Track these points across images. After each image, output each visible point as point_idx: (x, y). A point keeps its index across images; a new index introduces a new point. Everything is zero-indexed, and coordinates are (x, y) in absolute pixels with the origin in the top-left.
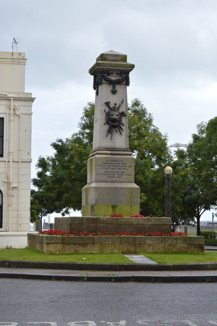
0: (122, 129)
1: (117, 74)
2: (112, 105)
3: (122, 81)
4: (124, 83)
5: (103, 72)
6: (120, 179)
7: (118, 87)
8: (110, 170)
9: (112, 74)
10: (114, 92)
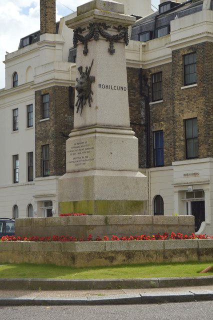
0: (91, 99)
1: (114, 28)
2: (84, 70)
3: (120, 39)
4: (122, 41)
5: (100, 24)
7: (117, 47)
8: (77, 156)
9: (109, 27)
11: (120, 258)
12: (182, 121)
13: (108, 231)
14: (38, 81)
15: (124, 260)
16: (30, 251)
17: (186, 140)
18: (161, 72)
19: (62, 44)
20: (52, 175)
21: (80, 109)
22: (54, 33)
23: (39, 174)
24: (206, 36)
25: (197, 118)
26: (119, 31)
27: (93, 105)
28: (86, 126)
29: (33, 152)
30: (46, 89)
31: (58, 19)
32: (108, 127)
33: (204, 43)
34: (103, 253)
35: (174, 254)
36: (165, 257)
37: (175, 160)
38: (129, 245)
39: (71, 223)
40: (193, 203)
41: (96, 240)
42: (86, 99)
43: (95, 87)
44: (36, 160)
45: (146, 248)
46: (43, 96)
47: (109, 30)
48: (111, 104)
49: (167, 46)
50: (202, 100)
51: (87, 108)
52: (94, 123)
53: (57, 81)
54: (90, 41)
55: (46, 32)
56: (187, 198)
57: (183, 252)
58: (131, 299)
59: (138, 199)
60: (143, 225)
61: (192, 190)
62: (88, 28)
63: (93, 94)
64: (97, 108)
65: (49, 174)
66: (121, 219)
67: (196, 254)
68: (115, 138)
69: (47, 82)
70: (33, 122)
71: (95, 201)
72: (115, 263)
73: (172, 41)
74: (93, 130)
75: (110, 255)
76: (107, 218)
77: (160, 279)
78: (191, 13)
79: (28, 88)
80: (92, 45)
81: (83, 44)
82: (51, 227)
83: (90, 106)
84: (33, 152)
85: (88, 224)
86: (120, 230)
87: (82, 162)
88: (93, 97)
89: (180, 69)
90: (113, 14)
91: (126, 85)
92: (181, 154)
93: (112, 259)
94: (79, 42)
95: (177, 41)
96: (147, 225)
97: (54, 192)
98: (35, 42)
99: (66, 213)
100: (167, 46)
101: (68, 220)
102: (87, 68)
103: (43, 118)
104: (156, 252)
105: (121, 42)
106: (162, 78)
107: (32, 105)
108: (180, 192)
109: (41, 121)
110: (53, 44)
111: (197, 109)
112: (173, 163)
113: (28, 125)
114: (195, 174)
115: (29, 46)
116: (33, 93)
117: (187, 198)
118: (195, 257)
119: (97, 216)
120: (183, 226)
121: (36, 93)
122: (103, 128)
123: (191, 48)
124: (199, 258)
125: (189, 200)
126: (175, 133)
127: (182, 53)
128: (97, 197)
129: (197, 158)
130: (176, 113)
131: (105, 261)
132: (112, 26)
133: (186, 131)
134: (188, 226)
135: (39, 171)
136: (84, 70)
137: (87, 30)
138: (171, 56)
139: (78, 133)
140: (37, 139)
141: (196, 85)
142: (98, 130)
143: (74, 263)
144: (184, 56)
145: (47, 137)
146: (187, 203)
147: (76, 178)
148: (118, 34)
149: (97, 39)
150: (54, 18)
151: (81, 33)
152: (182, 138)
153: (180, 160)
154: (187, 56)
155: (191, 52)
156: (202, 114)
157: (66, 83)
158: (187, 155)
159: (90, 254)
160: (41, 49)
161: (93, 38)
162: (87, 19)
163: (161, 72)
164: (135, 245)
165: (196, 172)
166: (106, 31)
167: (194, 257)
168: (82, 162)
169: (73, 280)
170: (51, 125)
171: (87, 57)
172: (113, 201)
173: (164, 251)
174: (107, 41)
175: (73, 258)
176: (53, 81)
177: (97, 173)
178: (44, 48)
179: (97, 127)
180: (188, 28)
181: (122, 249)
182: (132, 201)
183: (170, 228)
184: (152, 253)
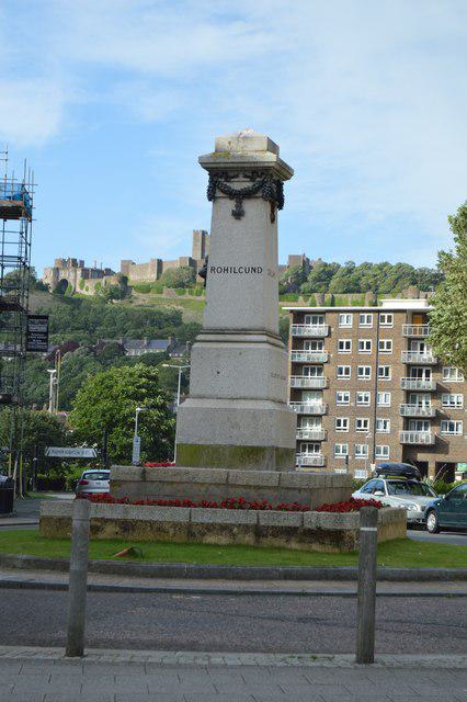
1: (246, 176)
32: (245, 331)
35: (209, 530)
36: (191, 534)
59: (255, 444)
72: (101, 536)
76: (144, 471)
82: (155, 484)
86: (168, 490)
96: (217, 485)
104: (175, 525)
118: (249, 539)
120: (287, 488)
124: (257, 541)
134: (300, 490)
172: (208, 446)
182: (245, 448)
184: (167, 526)
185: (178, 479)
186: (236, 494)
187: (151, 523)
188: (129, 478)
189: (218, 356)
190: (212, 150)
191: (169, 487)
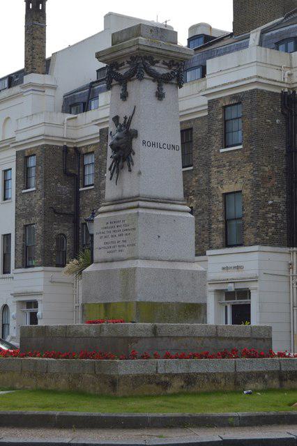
0: (132, 161)
1: (164, 63)
2: (122, 121)
4: (174, 81)
5: (146, 58)
6: (122, 255)
7: (167, 89)
8: (110, 239)
9: (158, 62)
10: (124, 96)
11: (177, 384)
12: (220, 195)
13: (156, 347)
14: (21, 137)
15: (182, 387)
16: (47, 372)
17: (226, 221)
18: (191, 129)
19: (54, 88)
20: (37, 266)
21: (115, 175)
22: (43, 74)
23: (20, 264)
24: (256, 82)
25: (241, 191)
26: (170, 68)
27: (135, 169)
28: (125, 199)
29: (10, 234)
30: (31, 148)
31: (48, 55)
32: (155, 200)
33: (253, 91)
34: (154, 376)
36: (237, 383)
37: (211, 248)
38: (189, 366)
39: (105, 333)
40: (234, 307)
41: (143, 357)
42: (124, 160)
43: (137, 144)
44: (16, 245)
45: (212, 370)
46: (27, 158)
47: (157, 66)
48: (158, 169)
49: (202, 94)
50: (249, 167)
51: (125, 174)
52: (135, 193)
53: (47, 138)
54: (130, 81)
55: (32, 72)
56: (226, 300)
57: (259, 375)
58: (230, 440)
60: (205, 337)
61: (233, 290)
62: (128, 62)
63: (134, 154)
64: (140, 173)
65: (34, 264)
66: (175, 328)
67: (276, 379)
68: (163, 215)
69: (34, 140)
70: (12, 193)
71: (137, 303)
72: (170, 391)
73: (208, 87)
74: (135, 204)
75: (163, 379)
76: (155, 328)
77: (240, 414)
78: (233, 51)
79: (6, 146)
80: (133, 87)
81: (120, 84)
82: (164, 339)
83: (130, 171)
84: (10, 234)
85: (131, 335)
86: (174, 344)
87: (117, 248)
88: (134, 158)
89: (218, 125)
90: (163, 44)
91: (179, 143)
92: (219, 240)
93: (166, 385)
94: (114, 82)
95: (216, 87)
96: (210, 338)
97: (39, 289)
98: (16, 84)
99: (94, 319)
100: (202, 94)
101: (101, 329)
102: (126, 118)
103: (27, 188)
104: (225, 375)
105: (172, 83)
106: (191, 136)
107: (11, 169)
108: (217, 291)
109: (24, 191)
110: (42, 88)
111: (241, 180)
112: (208, 252)
113: (5, 196)
114: (238, 268)
115: (8, 90)
116: (13, 152)
117: (226, 300)
118: (275, 383)
119: (143, 324)
120: (257, 339)
121: (18, 153)
122: (148, 201)
123: (234, 97)
124: (281, 385)
125: (228, 303)
126: (210, 212)
127: (222, 103)
128: (140, 297)
129: (241, 245)
130: (212, 185)
131: (156, 387)
132: (161, 62)
133: (225, 209)
135: (20, 259)
136: (122, 121)
137: (126, 65)
138: (207, 107)
139: (112, 207)
140: (18, 216)
141: (241, 147)
142: (141, 203)
143: (114, 390)
144: (224, 107)
145: (31, 214)
146: (226, 307)
147: (108, 272)
148: (169, 71)
149: (141, 78)
150: (44, 53)
151: (118, 69)
152: (221, 218)
153: (218, 248)
154: (229, 108)
155: (235, 102)
156: (249, 186)
157: (59, 141)
158: (226, 241)
159: (136, 378)
160: (25, 94)
161: (135, 77)
162: (127, 51)
163: (191, 129)
164: (198, 367)
165: (240, 264)
166: (153, 68)
167: (274, 383)
168: (117, 248)
169: (119, 415)
170: (38, 198)
171: (125, 103)
172: (161, 303)
173: (236, 374)
174: (154, 81)
175: (113, 383)
176: (42, 137)
177: (140, 264)
178: (29, 93)
179: (141, 200)
180: (272, 67)
181: (180, 371)
182: (187, 304)
183: (240, 342)
184: (219, 377)
185: (180, 334)
186: (224, 345)
187: (207, 375)
188: (144, 334)
189: (158, 222)
190: (99, 27)
191: (175, 341)
